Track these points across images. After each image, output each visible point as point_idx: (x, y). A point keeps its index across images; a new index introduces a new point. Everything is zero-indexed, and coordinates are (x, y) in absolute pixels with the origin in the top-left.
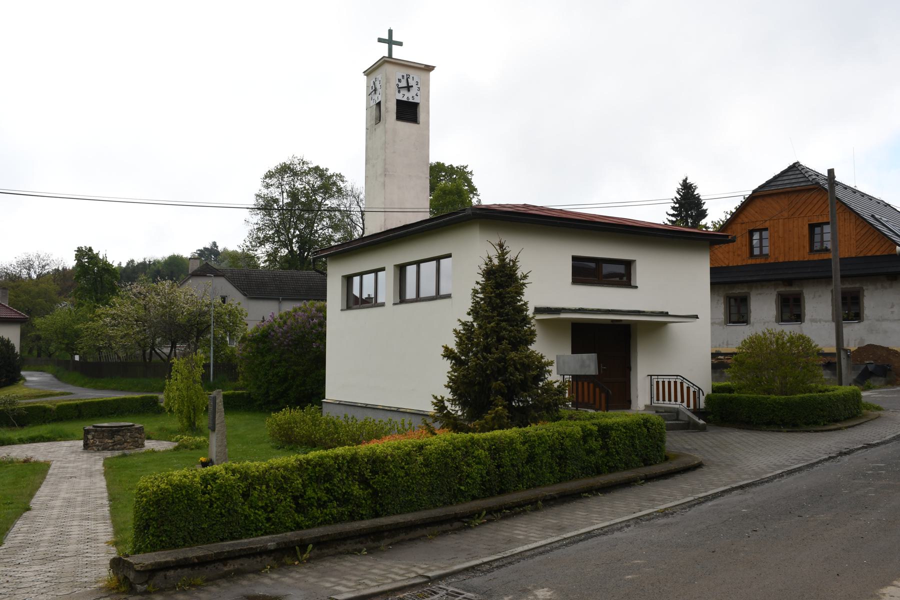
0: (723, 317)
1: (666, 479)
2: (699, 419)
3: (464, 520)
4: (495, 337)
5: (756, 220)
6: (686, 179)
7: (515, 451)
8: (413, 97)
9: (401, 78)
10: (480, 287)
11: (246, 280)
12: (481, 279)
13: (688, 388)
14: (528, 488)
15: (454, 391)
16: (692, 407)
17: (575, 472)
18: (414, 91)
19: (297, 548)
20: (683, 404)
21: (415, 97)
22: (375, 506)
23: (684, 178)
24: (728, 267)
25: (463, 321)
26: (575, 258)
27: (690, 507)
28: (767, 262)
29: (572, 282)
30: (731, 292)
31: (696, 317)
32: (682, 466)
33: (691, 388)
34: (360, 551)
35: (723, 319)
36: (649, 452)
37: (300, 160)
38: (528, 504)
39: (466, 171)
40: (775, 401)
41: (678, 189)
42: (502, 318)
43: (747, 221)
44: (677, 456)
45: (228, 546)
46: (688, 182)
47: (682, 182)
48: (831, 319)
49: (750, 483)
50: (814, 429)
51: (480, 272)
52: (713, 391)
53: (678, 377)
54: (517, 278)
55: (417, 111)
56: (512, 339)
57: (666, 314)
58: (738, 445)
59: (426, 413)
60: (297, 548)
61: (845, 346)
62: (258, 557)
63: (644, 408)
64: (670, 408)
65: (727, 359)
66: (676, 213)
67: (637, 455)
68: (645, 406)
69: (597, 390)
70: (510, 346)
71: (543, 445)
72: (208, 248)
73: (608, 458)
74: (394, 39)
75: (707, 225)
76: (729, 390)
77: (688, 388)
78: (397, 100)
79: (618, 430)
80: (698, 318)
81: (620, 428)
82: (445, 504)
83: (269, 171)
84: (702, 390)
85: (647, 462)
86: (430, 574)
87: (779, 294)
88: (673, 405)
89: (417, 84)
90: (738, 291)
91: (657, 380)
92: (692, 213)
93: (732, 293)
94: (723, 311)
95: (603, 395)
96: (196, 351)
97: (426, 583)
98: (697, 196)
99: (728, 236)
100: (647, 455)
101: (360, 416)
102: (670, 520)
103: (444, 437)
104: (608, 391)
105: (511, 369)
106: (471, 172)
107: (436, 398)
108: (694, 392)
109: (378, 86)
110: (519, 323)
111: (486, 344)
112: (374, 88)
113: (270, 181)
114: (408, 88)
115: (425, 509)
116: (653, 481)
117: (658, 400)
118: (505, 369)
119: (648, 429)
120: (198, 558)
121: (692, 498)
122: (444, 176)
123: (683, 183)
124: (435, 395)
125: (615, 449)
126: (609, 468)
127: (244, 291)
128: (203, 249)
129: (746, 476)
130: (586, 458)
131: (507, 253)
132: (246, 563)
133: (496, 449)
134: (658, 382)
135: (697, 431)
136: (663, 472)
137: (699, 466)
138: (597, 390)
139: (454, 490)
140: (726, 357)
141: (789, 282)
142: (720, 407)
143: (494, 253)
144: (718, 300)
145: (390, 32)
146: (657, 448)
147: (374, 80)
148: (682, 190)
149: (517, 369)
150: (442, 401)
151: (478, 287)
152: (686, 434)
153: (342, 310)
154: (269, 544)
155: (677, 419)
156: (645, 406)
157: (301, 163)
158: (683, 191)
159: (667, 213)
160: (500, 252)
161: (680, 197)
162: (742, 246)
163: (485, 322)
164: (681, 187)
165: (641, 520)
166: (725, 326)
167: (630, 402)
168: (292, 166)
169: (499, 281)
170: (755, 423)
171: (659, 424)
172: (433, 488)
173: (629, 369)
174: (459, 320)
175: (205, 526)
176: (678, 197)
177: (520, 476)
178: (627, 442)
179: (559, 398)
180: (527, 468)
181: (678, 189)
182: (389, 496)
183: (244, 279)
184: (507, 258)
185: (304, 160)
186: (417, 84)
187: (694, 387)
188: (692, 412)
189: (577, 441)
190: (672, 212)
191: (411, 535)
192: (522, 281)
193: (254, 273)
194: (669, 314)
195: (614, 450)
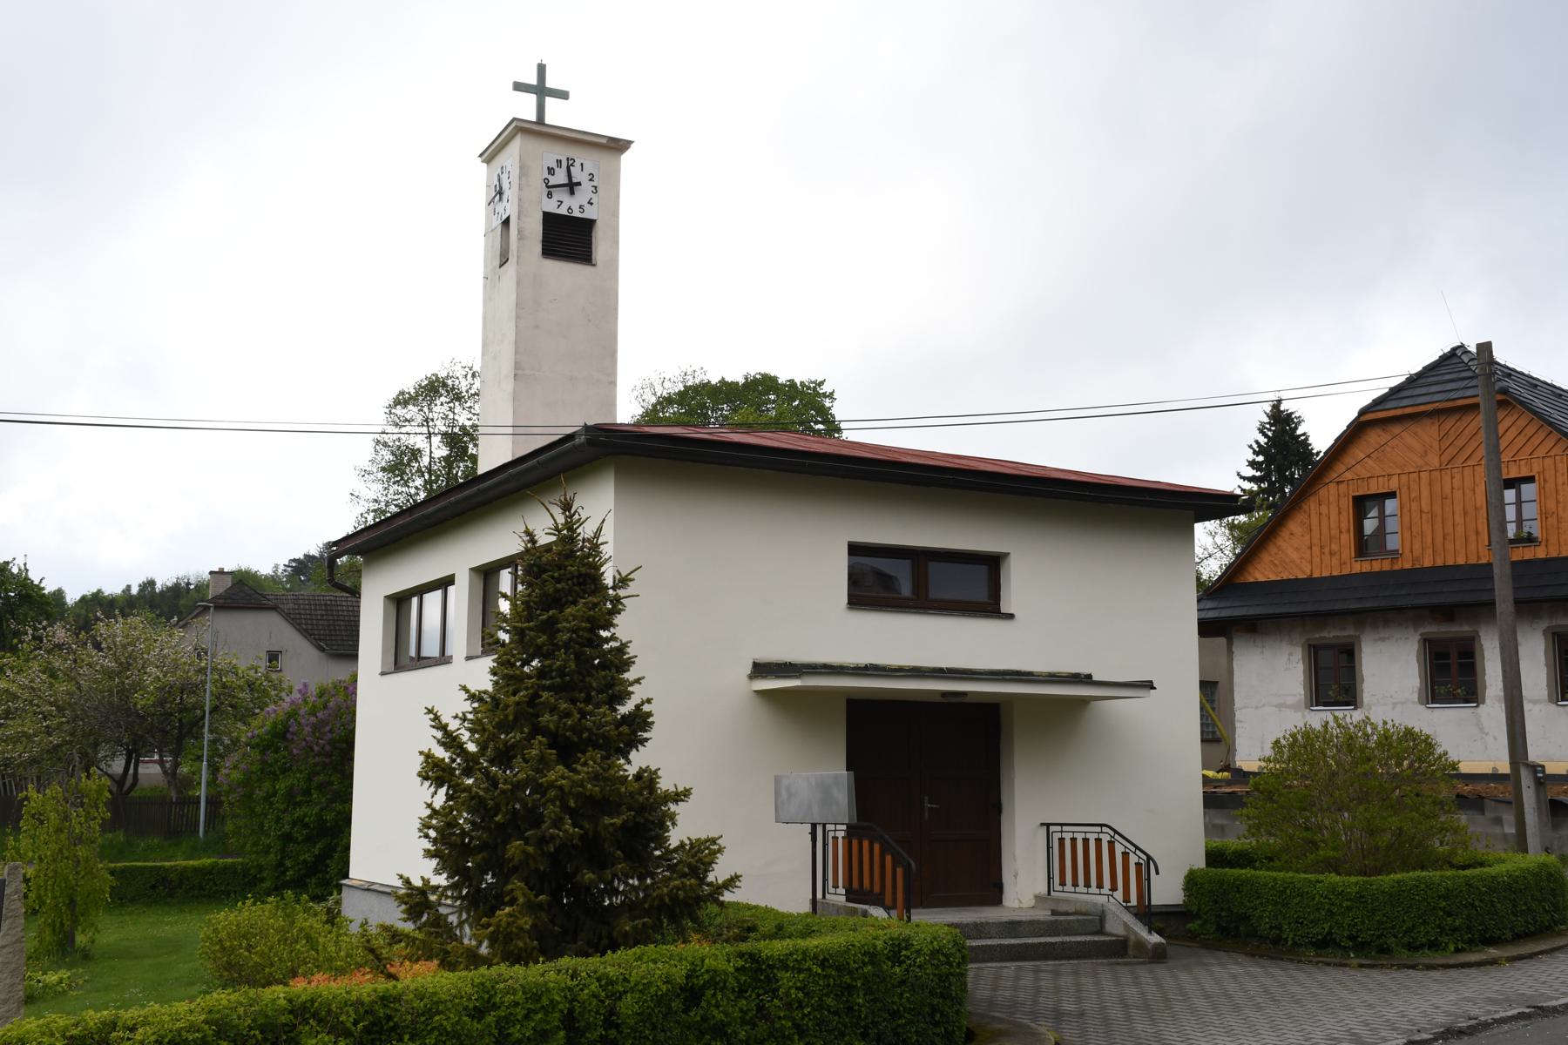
0: (1303, 692)
2: (1150, 932)
5: (1369, 475)
9: (554, 165)
11: (325, 618)
13: (1125, 855)
20: (1115, 894)
21: (587, 207)
24: (1310, 580)
25: (473, 691)
26: (855, 549)
28: (1396, 567)
29: (848, 603)
30: (1317, 636)
31: (1150, 685)
35: (1303, 697)
36: (903, 1026)
37: (467, 369)
39: (821, 392)
40: (1333, 889)
41: (1262, 424)
43: (1350, 478)
46: (1282, 408)
48: (1546, 697)
50: (1426, 961)
52: (1208, 864)
53: (1105, 829)
55: (591, 237)
57: (1086, 680)
61: (1534, 755)
63: (1032, 903)
66: (1258, 474)
68: (1036, 897)
69: (889, 858)
72: (314, 557)
74: (550, 84)
76: (1243, 859)
77: (1125, 855)
78: (544, 212)
79: (800, 971)
80: (1155, 688)
81: (809, 963)
83: (402, 393)
87: (1425, 640)
89: (591, 180)
90: (1331, 634)
91: (1059, 835)
92: (1293, 474)
93: (1321, 637)
95: (899, 871)
96: (88, 771)
98: (1303, 438)
100: (896, 1034)
104: (909, 864)
106: (832, 394)
108: (1138, 864)
109: (505, 186)
113: (405, 411)
114: (572, 186)
117: (1063, 883)
122: (774, 401)
123: (1272, 411)
127: (320, 640)
128: (302, 557)
134: (1062, 840)
141: (1446, 613)
144: (1290, 654)
145: (541, 69)
147: (499, 171)
148: (1271, 425)
155: (1101, 932)
156: (1036, 897)
157: (469, 376)
159: (1238, 474)
161: (1266, 440)
162: (1341, 532)
164: (1267, 420)
168: (449, 382)
174: (464, 688)
176: (1263, 440)
181: (1262, 424)
183: (322, 615)
185: (474, 369)
186: (591, 180)
187: (1138, 852)
188: (1136, 915)
190: (1250, 472)
193: (344, 603)
194: (1095, 678)
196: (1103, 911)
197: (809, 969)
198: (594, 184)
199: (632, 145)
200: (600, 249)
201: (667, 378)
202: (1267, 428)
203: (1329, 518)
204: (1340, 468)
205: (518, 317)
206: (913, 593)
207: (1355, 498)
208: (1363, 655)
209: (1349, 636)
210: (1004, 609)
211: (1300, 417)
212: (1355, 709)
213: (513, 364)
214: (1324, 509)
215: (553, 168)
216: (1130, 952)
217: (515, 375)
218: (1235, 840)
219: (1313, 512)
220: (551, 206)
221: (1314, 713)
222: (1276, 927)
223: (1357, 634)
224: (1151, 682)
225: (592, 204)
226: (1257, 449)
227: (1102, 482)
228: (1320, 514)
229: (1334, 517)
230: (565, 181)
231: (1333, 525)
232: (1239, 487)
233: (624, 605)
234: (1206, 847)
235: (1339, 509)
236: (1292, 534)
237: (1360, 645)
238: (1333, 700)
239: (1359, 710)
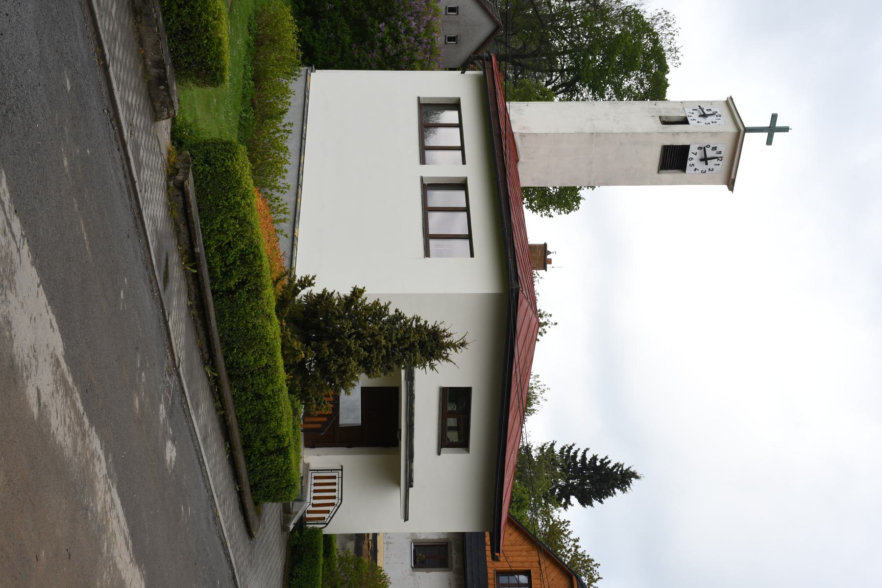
0: (421, 538)
1: (240, 509)
2: (294, 524)
3: (210, 361)
4: (371, 344)
6: (637, 477)
7: (266, 386)
8: (693, 165)
9: (718, 150)
10: (423, 325)
12: (430, 324)
13: (328, 512)
14: (233, 396)
15: (321, 297)
16: (308, 516)
17: (246, 430)
18: (701, 166)
19: (195, 263)
21: (694, 168)
22: (220, 292)
23: (638, 474)
25: (389, 307)
27: (220, 537)
29: (443, 388)
30: (453, 547)
32: (251, 521)
33: (328, 515)
34: (190, 300)
35: (419, 538)
36: (264, 489)
38: (221, 404)
41: (622, 466)
42: (390, 350)
44: (259, 514)
45: (194, 209)
46: (632, 479)
47: (632, 471)
49: (237, 584)
51: (438, 323)
52: (325, 536)
53: (340, 501)
54: (430, 360)
55: (676, 169)
56: (370, 359)
57: (410, 483)
58: (269, 568)
59: (297, 225)
60: (195, 263)
62: (189, 242)
63: (306, 462)
64: (307, 492)
65: (368, 543)
66: (588, 462)
67: (260, 479)
70: (363, 359)
71: (271, 406)
73: (258, 455)
75: (569, 506)
77: (328, 512)
78: (689, 146)
79: (284, 463)
82: (221, 338)
84: (326, 526)
85: (254, 487)
86: (181, 368)
88: (310, 495)
89: (709, 169)
91: (337, 476)
92: (587, 484)
93: (452, 549)
94: (430, 538)
95: (319, 426)
97: (175, 367)
99: (499, 552)
100: (261, 487)
101: (292, 144)
102: (212, 523)
103: (270, 295)
104: (323, 432)
105: (340, 361)
107: (313, 278)
108: (324, 518)
109: (709, 119)
110: (386, 365)
111: (364, 336)
112: (707, 113)
114: (705, 160)
115: (218, 326)
116: (238, 498)
117: (315, 478)
118: (341, 355)
119: (285, 488)
120: (191, 212)
121: (226, 536)
123: (631, 472)
124: (315, 278)
125: (267, 462)
126: (249, 456)
129: (242, 580)
130: (259, 439)
131: (456, 351)
132: (184, 236)
133: (267, 371)
134: (334, 477)
135: (282, 522)
136: (246, 505)
137: (250, 534)
138: (325, 419)
139: (233, 345)
140: (370, 543)
142: (308, 545)
143: (455, 339)
145: (786, 129)
146: (267, 496)
149: (340, 366)
150: (310, 284)
151: (422, 323)
152: (279, 512)
153: (419, 98)
154: (198, 248)
158: (619, 473)
159: (587, 449)
160: (456, 344)
161: (610, 468)
163: (386, 333)
164: (625, 469)
165: (212, 499)
166: (410, 540)
167: (313, 446)
169: (427, 345)
170: (291, 582)
171: (290, 497)
172: (235, 330)
173: (349, 446)
174: (390, 303)
175: (210, 197)
176: (610, 466)
177: (244, 389)
178: (273, 471)
179: (313, 404)
180: (250, 394)
181: (622, 466)
182: (229, 302)
184: (451, 350)
186: (709, 169)
187: (330, 518)
188: (302, 516)
189: (274, 431)
190: (589, 456)
191: (200, 328)
192: (428, 364)
194: (410, 488)
195: (265, 461)
196: (303, 501)
197: (284, 466)
198: (707, 172)
199: (731, 192)
200: (668, 175)
201: (675, 37)
202: (619, 468)
203: (519, 556)
204: (547, 563)
205: (627, 134)
206: (449, 411)
207: (530, 570)
208: (442, 572)
209: (452, 565)
210: (443, 450)
211: (626, 490)
212: (412, 567)
213: (599, 132)
214: (524, 553)
215: (716, 149)
216: (285, 515)
217: (593, 134)
218: (337, 545)
219: (522, 547)
220: (693, 149)
221: (410, 544)
222: (297, 576)
223: (453, 570)
224: (408, 520)
225: (695, 170)
226: (604, 462)
227: (504, 495)
228: (521, 551)
229: (519, 559)
230: (708, 156)
231: (515, 558)
232: (579, 449)
233: (422, 369)
234: (333, 535)
235: (524, 562)
236: (511, 535)
237: (447, 571)
238: (417, 555)
239: (411, 569)
